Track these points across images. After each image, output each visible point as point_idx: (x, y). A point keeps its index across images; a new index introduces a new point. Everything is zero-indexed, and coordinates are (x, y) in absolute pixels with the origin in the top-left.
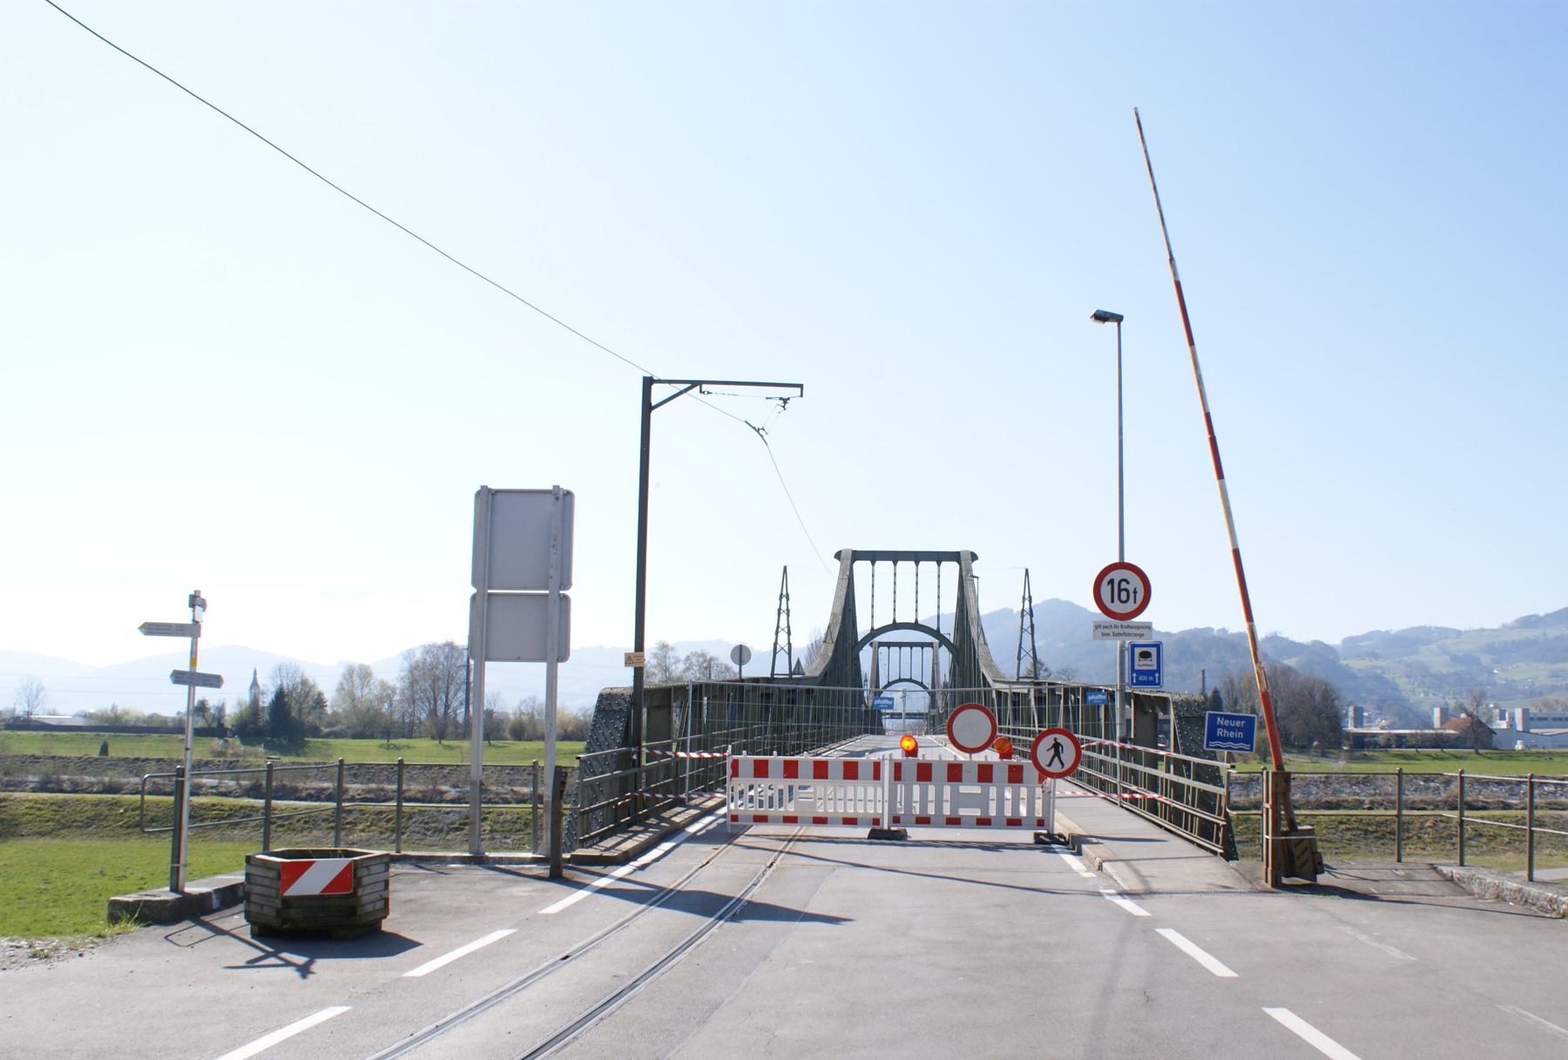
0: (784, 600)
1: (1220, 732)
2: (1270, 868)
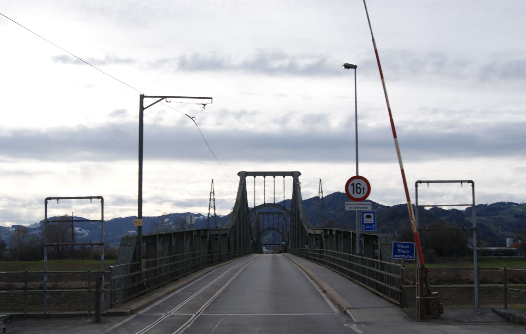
0: (212, 194)
1: (399, 251)
2: (419, 311)
